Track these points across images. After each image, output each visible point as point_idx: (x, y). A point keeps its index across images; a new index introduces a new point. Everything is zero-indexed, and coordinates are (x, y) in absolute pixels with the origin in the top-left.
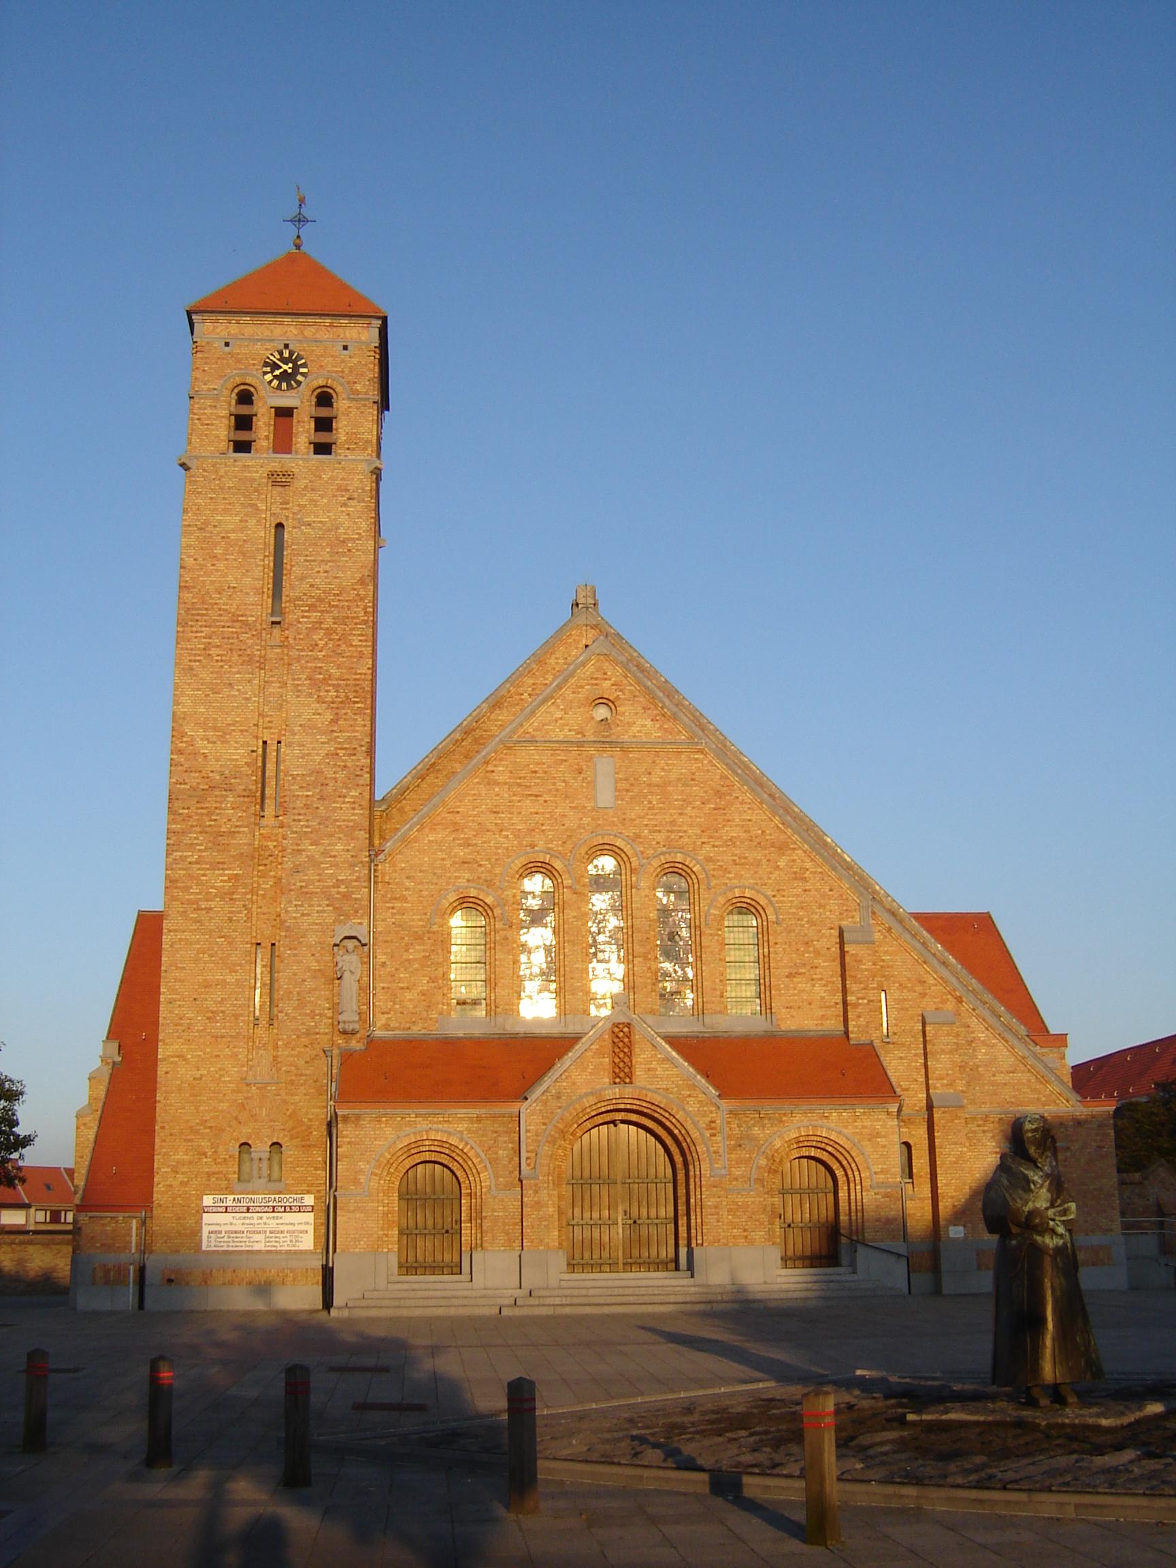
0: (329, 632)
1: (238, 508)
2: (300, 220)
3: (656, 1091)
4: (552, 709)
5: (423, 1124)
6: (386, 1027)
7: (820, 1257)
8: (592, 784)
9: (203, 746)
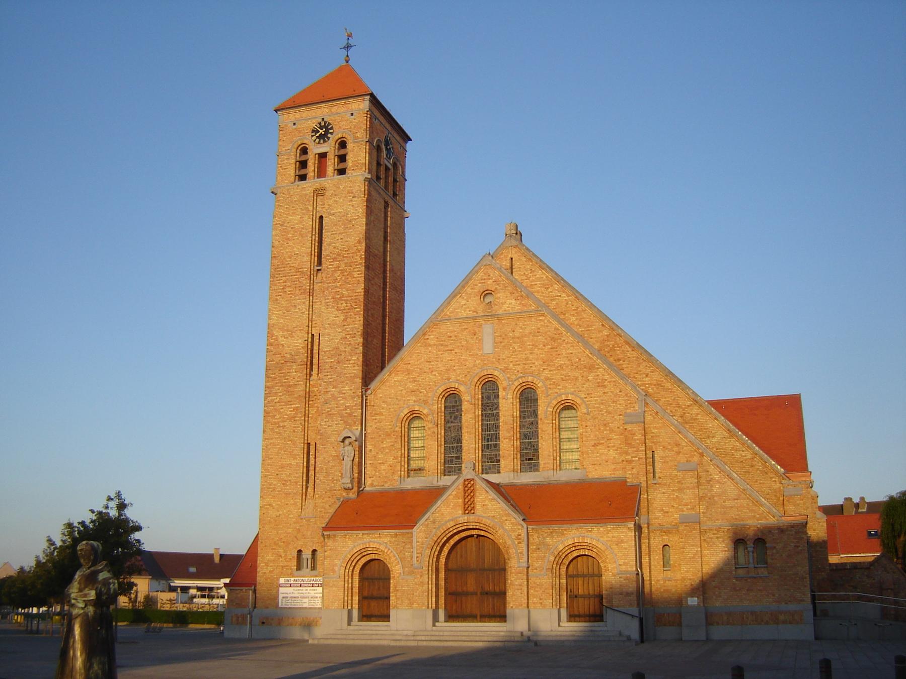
0: (343, 271)
1: (299, 211)
2: (348, 47)
3: (488, 518)
4: (460, 300)
5: (367, 539)
6: (372, 485)
7: (590, 616)
8: (481, 341)
9: (282, 340)
